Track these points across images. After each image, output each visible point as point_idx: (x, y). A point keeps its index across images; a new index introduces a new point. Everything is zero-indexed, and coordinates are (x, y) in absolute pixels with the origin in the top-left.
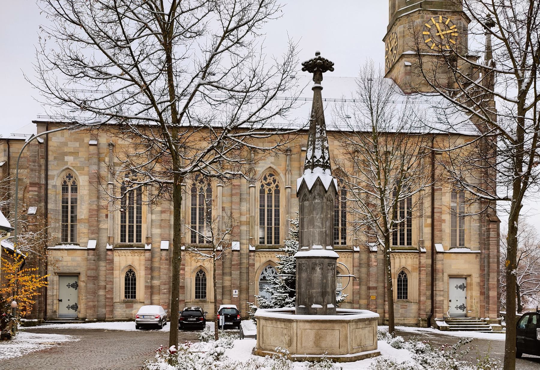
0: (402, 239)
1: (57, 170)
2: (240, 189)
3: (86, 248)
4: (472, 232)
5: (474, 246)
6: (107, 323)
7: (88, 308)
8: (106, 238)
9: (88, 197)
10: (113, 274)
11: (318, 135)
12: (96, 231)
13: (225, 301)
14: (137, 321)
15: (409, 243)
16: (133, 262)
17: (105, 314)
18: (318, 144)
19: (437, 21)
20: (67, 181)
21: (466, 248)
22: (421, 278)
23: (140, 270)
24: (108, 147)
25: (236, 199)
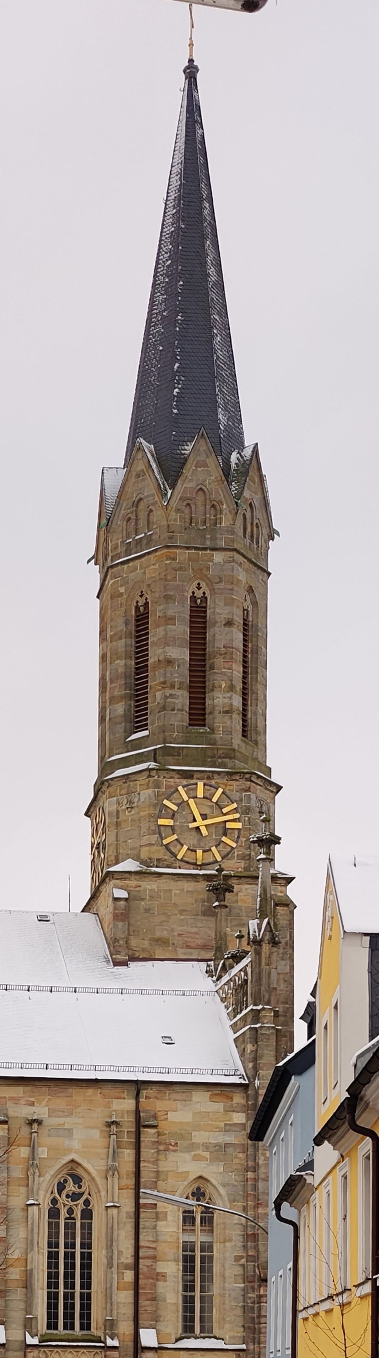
0: (69, 1316)
4: (227, 1302)
5: (232, 1334)
15: (86, 1326)
21: (215, 1337)
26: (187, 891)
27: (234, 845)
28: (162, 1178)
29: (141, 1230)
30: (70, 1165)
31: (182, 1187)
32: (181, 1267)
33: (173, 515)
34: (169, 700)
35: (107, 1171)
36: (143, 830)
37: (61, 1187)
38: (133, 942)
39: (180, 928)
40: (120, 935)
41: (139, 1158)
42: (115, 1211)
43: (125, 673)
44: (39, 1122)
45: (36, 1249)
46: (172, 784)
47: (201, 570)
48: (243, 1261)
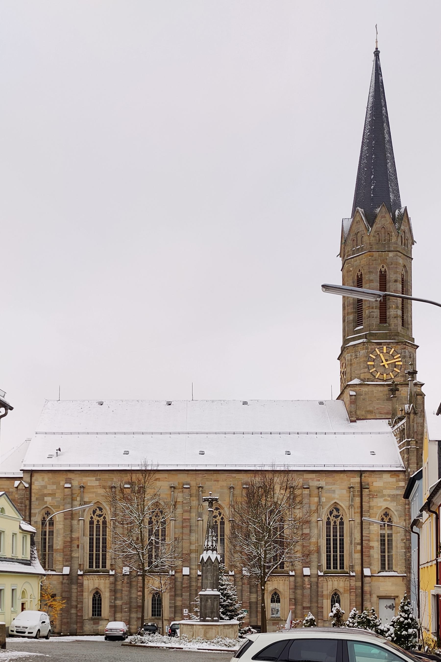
1: (38, 509)
2: (190, 522)
3: (61, 574)
4: (398, 557)
6: (78, 636)
7: (62, 624)
8: (78, 565)
9: (63, 530)
10: (82, 595)
11: (210, 534)
12: (69, 559)
13: (177, 618)
14: (106, 634)
15: (342, 567)
16: (99, 585)
17: (77, 629)
18: (210, 539)
19: (381, 351)
20: (46, 517)
21: (394, 571)
22: (351, 599)
23: (105, 592)
24: (79, 489)
25: (186, 531)
26: (380, 391)
27: (399, 371)
28: (371, 509)
29: (363, 529)
30: (335, 504)
31: (379, 512)
32: (380, 544)
33: (372, 238)
34: (371, 314)
35: (349, 506)
36: (361, 367)
37: (331, 513)
38: (358, 412)
39: (378, 406)
40: (353, 410)
41: (362, 501)
42: (353, 522)
43: (353, 303)
44: (322, 488)
45: (321, 537)
46: (373, 348)
47: (384, 260)
48: (405, 541)
